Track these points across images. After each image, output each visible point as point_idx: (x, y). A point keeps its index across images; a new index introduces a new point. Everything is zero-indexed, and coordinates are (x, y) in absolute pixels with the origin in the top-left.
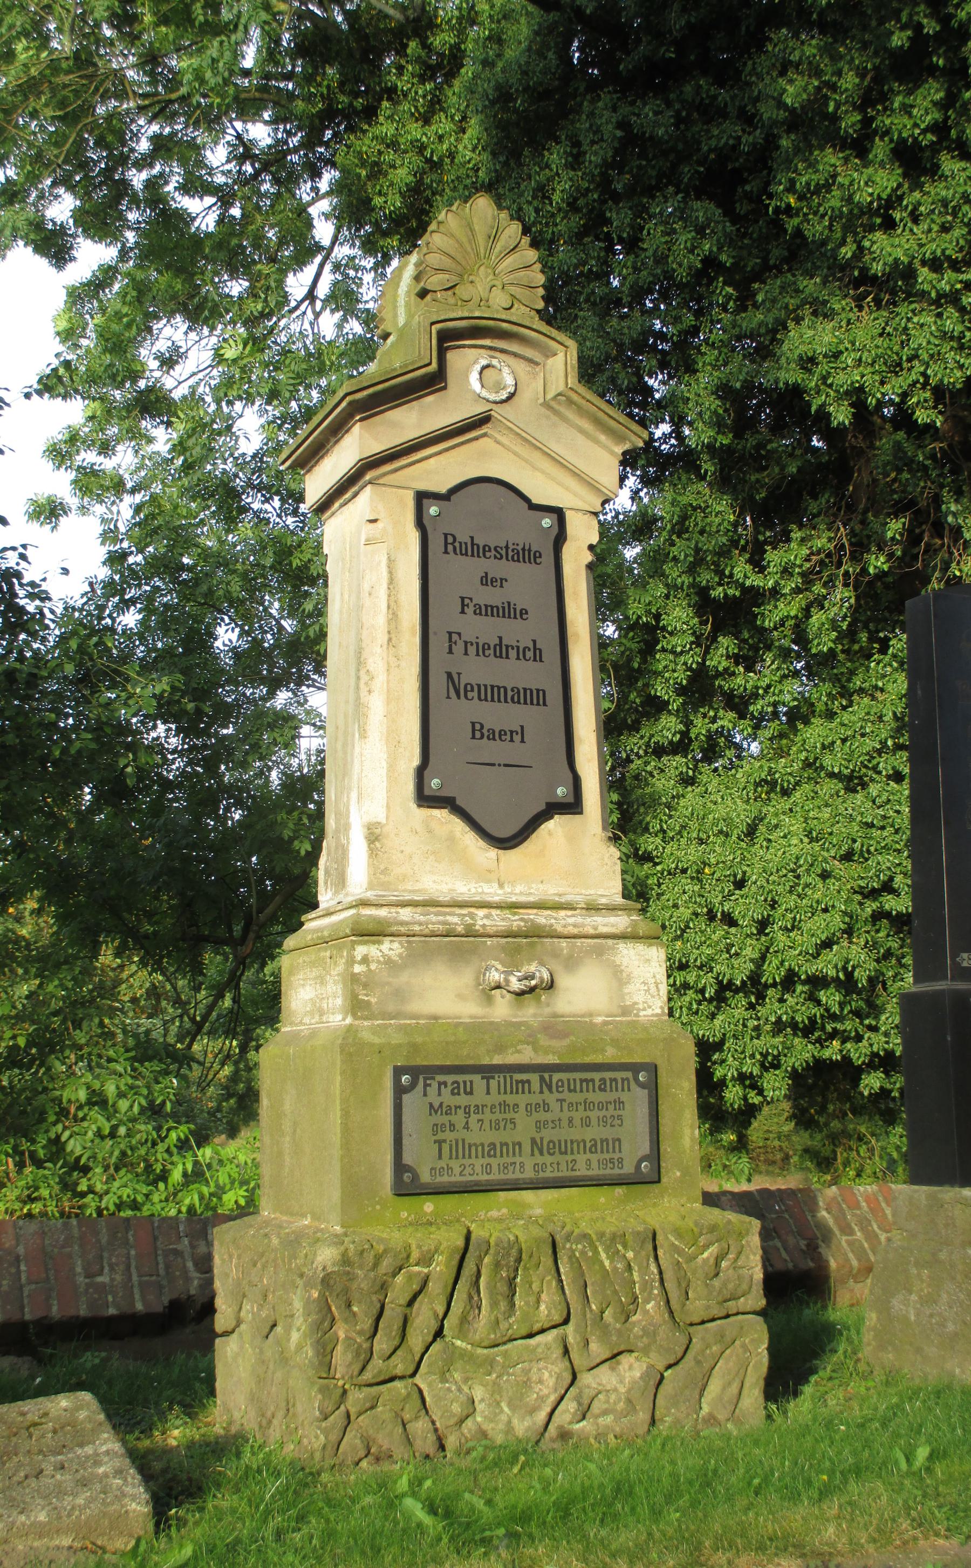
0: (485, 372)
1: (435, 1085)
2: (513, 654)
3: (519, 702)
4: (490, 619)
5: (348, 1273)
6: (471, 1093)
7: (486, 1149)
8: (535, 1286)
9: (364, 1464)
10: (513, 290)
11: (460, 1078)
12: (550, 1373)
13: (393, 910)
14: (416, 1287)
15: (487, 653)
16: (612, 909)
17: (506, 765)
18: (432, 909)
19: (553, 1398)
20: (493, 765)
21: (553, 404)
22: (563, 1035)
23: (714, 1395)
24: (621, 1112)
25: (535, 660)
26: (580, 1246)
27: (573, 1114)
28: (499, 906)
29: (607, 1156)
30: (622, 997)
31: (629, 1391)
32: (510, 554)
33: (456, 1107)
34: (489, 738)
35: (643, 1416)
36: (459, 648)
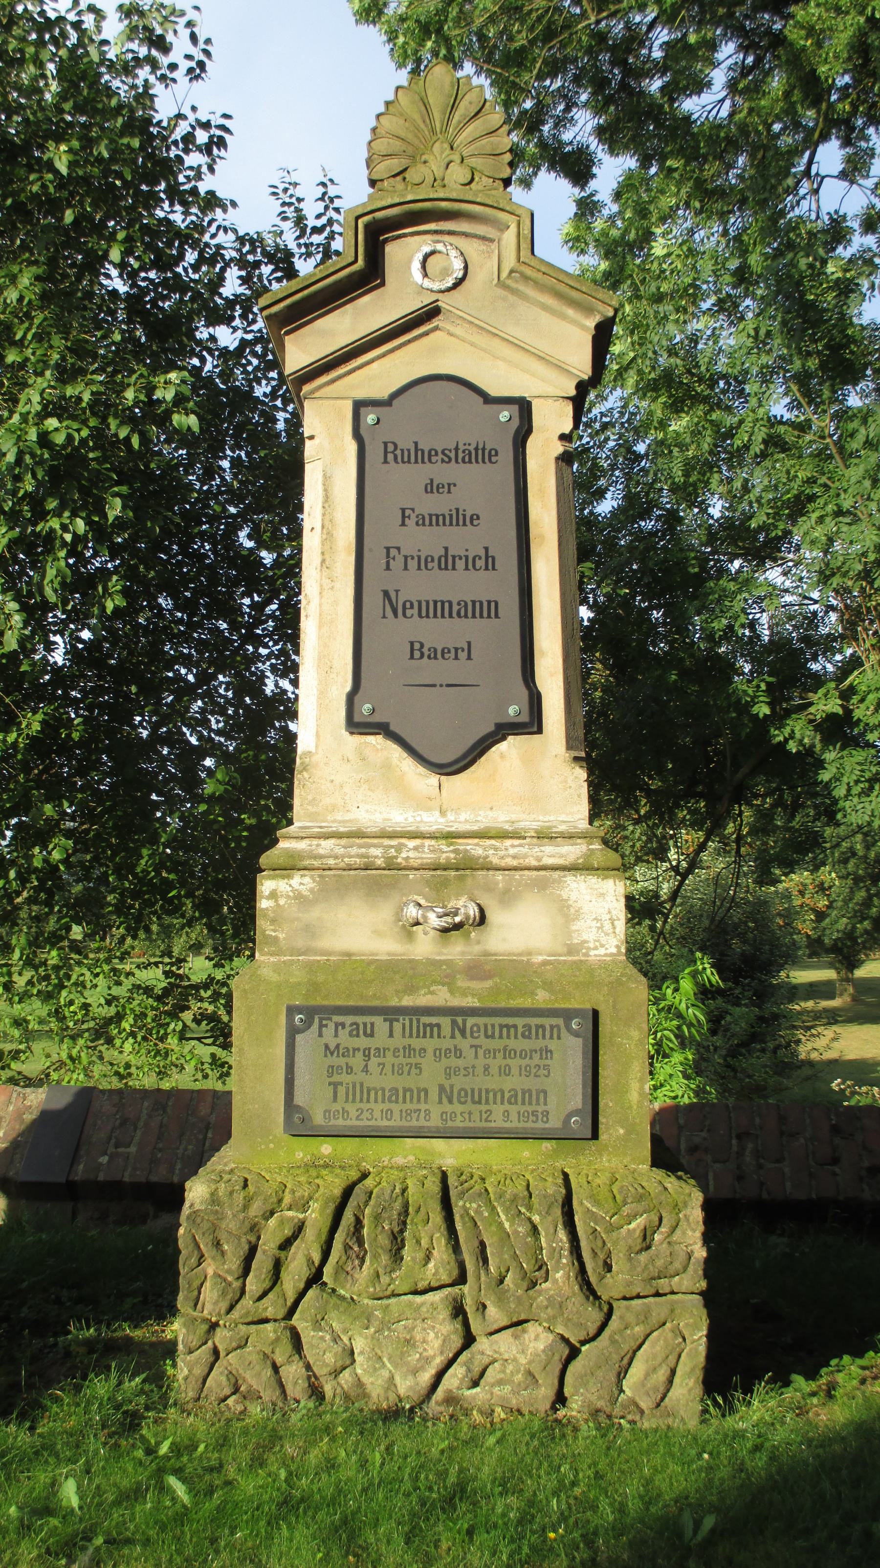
0: (431, 260)
1: (332, 1026)
2: (460, 564)
3: (466, 616)
4: (435, 528)
5: (217, 1212)
6: (372, 1035)
7: (387, 1094)
8: (424, 1242)
9: (230, 1401)
10: (473, 162)
11: (360, 1019)
12: (436, 1334)
13: (315, 842)
14: (288, 1232)
15: (430, 565)
16: (570, 837)
17: (448, 686)
18: (357, 841)
19: (438, 1361)
20: (434, 686)
21: (509, 282)
22: (488, 976)
23: (635, 1379)
24: (548, 1062)
25: (487, 569)
26: (474, 1205)
27: (490, 1061)
28: (432, 836)
29: (530, 1109)
30: (569, 935)
31: (530, 1362)
32: (461, 455)
33: (354, 1050)
34: (429, 657)
35: (545, 1392)
36: (397, 564)
